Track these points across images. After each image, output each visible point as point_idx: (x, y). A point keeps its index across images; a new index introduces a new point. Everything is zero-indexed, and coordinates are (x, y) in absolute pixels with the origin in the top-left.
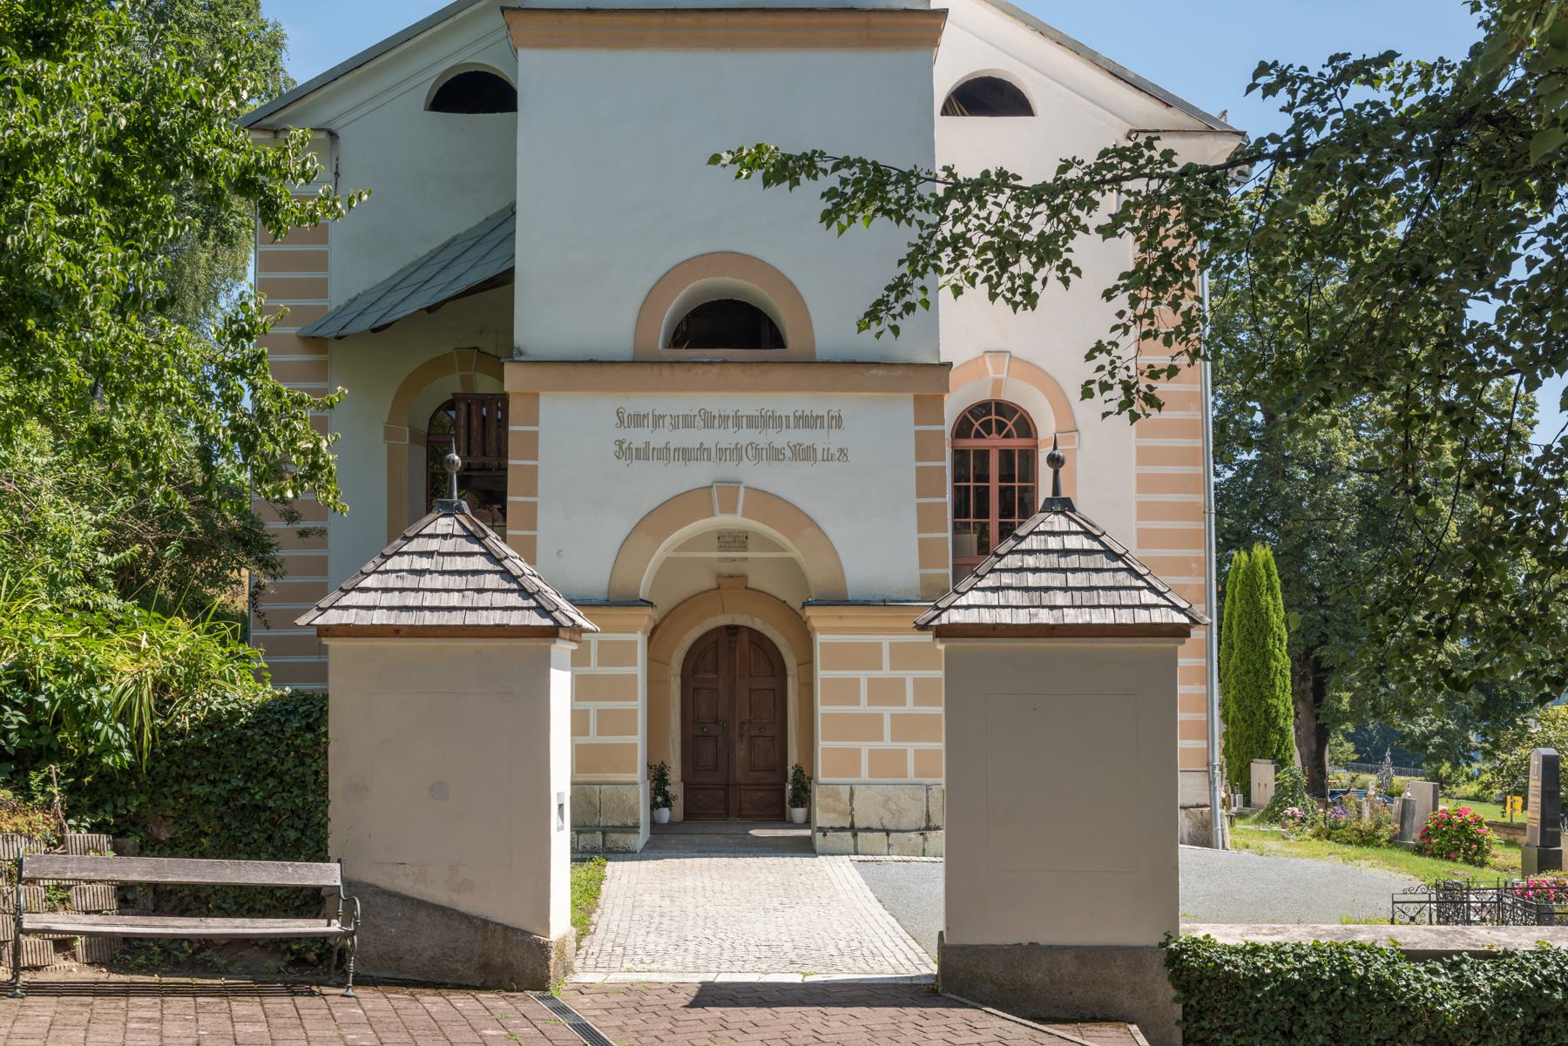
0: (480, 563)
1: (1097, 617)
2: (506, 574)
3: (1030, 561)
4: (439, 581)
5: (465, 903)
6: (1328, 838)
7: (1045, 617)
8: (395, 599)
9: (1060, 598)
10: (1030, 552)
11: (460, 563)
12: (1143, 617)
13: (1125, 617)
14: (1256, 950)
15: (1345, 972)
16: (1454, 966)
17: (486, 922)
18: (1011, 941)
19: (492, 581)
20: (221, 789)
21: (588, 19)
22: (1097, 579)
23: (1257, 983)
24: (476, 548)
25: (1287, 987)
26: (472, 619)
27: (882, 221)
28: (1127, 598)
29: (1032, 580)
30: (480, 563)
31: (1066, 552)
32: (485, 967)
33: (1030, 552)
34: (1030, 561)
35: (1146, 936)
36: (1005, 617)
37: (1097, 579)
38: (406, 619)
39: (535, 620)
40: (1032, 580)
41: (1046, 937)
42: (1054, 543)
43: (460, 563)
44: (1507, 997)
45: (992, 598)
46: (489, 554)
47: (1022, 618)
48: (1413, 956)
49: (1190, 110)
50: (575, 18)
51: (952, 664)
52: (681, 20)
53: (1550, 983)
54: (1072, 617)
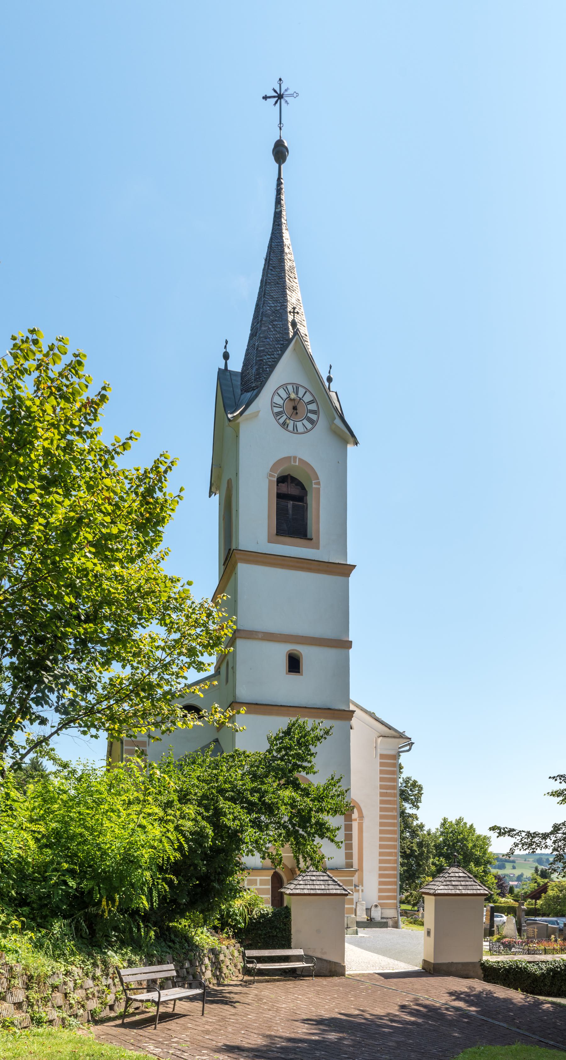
0: (326, 878)
1: (469, 892)
2: (334, 881)
3: (453, 879)
4: (318, 883)
5: (325, 957)
6: (414, 923)
7: (458, 892)
8: (309, 887)
9: (461, 888)
10: (452, 877)
11: (322, 878)
12: (479, 892)
13: (475, 892)
14: (498, 962)
15: (517, 967)
16: (537, 964)
17: (330, 961)
18: (447, 961)
19: (330, 882)
20: (264, 932)
21: (256, 706)
22: (467, 883)
23: (500, 969)
24: (325, 874)
25: (506, 969)
26: (328, 892)
27: (510, 838)
28: (474, 887)
29: (454, 883)
30: (326, 878)
31: (460, 877)
32: (330, 971)
33: (452, 877)
34: (453, 879)
35: (476, 960)
36: (450, 892)
37: (467, 883)
38: (312, 892)
39: (344, 892)
40: (454, 883)
41: (455, 961)
42: (457, 875)
43: (322, 878)
44: (549, 970)
45: (446, 887)
46: (328, 876)
47: (453, 892)
48: (530, 962)
49: (396, 731)
50: (253, 706)
51: (436, 901)
52: (282, 708)
53: (557, 967)
54: (464, 892)
